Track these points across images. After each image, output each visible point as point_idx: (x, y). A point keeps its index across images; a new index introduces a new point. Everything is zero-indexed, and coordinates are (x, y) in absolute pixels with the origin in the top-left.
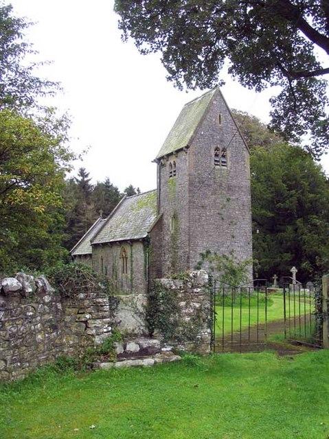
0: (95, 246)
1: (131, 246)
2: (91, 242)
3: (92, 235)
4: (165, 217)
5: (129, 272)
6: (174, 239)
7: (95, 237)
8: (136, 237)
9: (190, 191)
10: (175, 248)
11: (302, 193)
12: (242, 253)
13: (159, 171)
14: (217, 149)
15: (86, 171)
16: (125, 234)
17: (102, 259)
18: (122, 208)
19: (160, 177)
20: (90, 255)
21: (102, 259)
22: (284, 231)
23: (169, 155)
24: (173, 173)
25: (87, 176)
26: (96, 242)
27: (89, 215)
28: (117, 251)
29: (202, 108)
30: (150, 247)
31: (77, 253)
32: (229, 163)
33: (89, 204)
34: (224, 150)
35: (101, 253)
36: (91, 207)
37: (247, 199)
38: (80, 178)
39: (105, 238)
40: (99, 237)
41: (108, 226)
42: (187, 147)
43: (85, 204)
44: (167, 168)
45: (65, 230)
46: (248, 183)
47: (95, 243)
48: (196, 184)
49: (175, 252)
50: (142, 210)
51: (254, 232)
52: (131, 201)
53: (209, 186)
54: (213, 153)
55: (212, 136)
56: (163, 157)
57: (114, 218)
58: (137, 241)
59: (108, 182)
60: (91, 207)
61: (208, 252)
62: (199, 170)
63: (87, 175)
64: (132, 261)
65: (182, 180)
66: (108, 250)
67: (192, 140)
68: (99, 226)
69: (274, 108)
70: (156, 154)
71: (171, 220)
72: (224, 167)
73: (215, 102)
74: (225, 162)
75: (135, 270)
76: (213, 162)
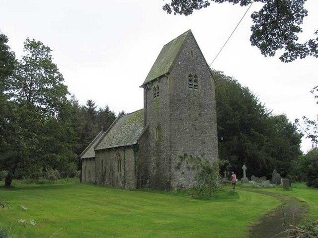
0: (97, 152)
1: (124, 151)
2: (94, 148)
3: (96, 143)
4: (151, 128)
5: (123, 171)
6: (158, 145)
7: (98, 144)
8: (128, 144)
9: (170, 107)
10: (158, 152)
11: (243, 113)
12: (212, 158)
13: (146, 94)
14: (190, 76)
15: (93, 102)
16: (120, 142)
17: (102, 161)
18: (117, 124)
19: (146, 98)
20: (94, 158)
21: (102, 161)
22: (230, 140)
23: (153, 81)
24: (157, 95)
25: (93, 105)
26: (98, 148)
27: (94, 131)
28: (114, 155)
29: (179, 44)
30: (139, 151)
31: (84, 157)
32: (200, 87)
33: (94, 124)
34: (196, 77)
35: (102, 157)
36: (96, 125)
37: (213, 113)
38: (88, 107)
39: (104, 145)
40: (100, 144)
41: (107, 137)
42: (168, 73)
43: (92, 124)
44: (152, 91)
45: (78, 141)
46: (214, 102)
47: (97, 149)
48: (175, 102)
49: (159, 155)
50: (133, 124)
51: (219, 140)
52: (123, 118)
53: (185, 103)
54: (188, 78)
55: (187, 66)
56: (148, 83)
57: (111, 131)
58: (129, 147)
59: (107, 109)
60: (96, 125)
61: (185, 155)
62: (177, 91)
63: (93, 104)
64: (125, 163)
65: (164, 100)
66: (106, 154)
67: (171, 69)
68: (100, 138)
69: (256, 23)
70: (142, 81)
71: (155, 131)
72: (196, 89)
73: (188, 41)
74: (196, 86)
75: (127, 169)
76: (188, 86)
